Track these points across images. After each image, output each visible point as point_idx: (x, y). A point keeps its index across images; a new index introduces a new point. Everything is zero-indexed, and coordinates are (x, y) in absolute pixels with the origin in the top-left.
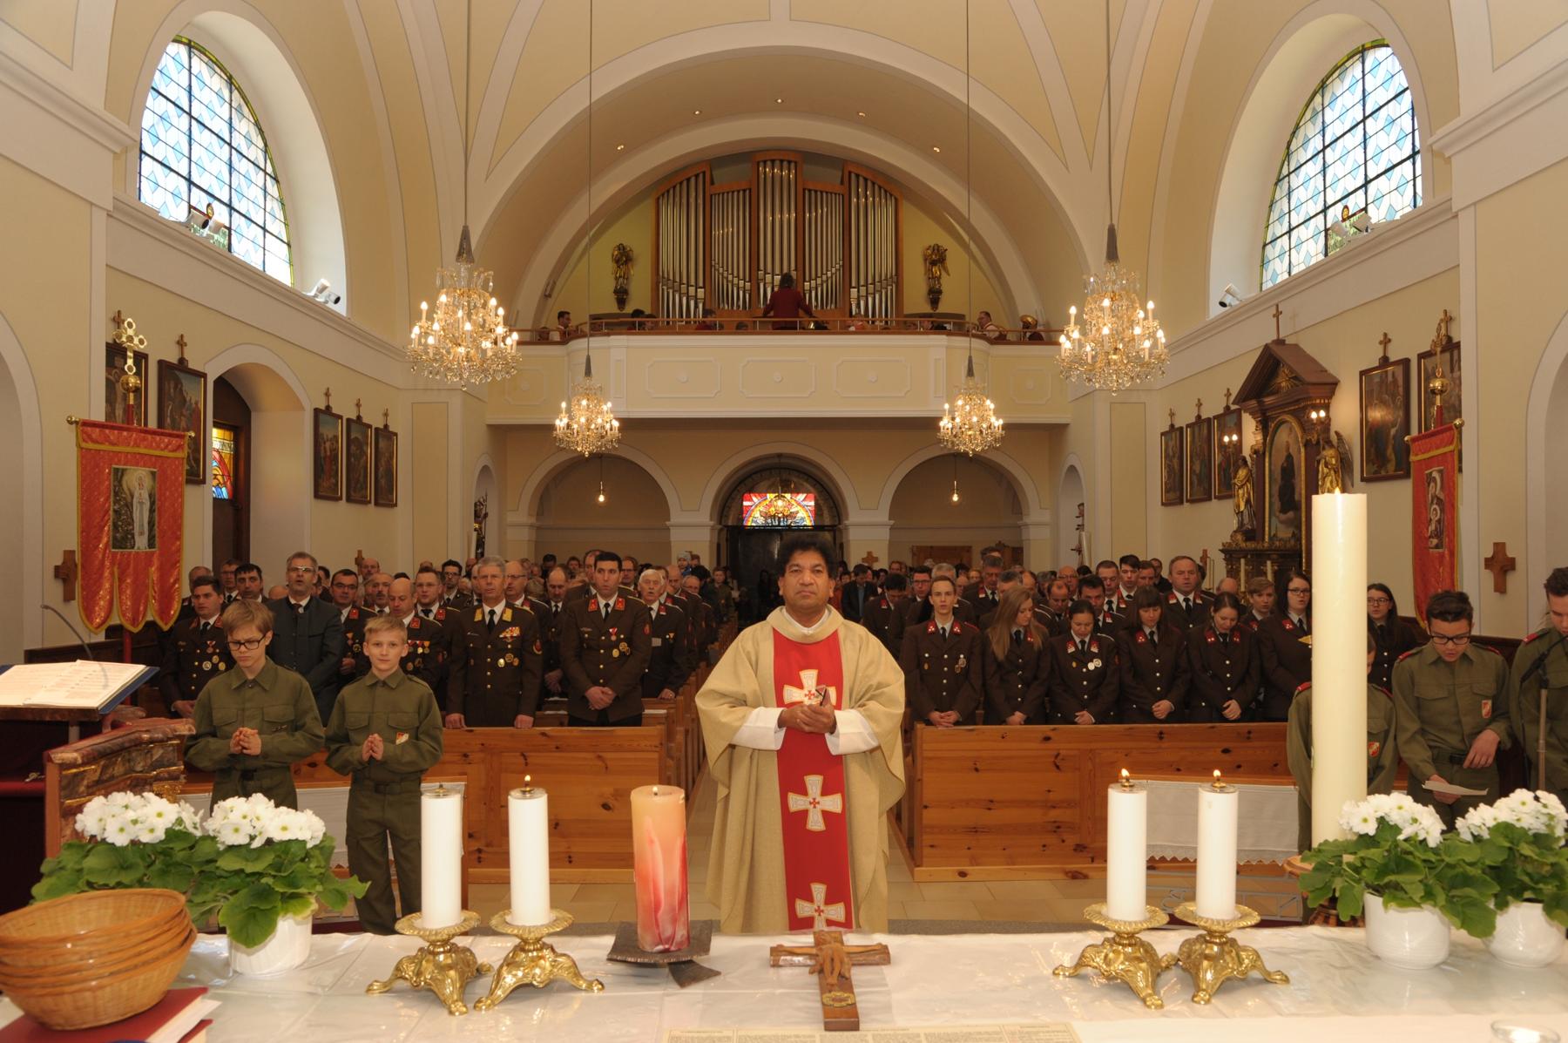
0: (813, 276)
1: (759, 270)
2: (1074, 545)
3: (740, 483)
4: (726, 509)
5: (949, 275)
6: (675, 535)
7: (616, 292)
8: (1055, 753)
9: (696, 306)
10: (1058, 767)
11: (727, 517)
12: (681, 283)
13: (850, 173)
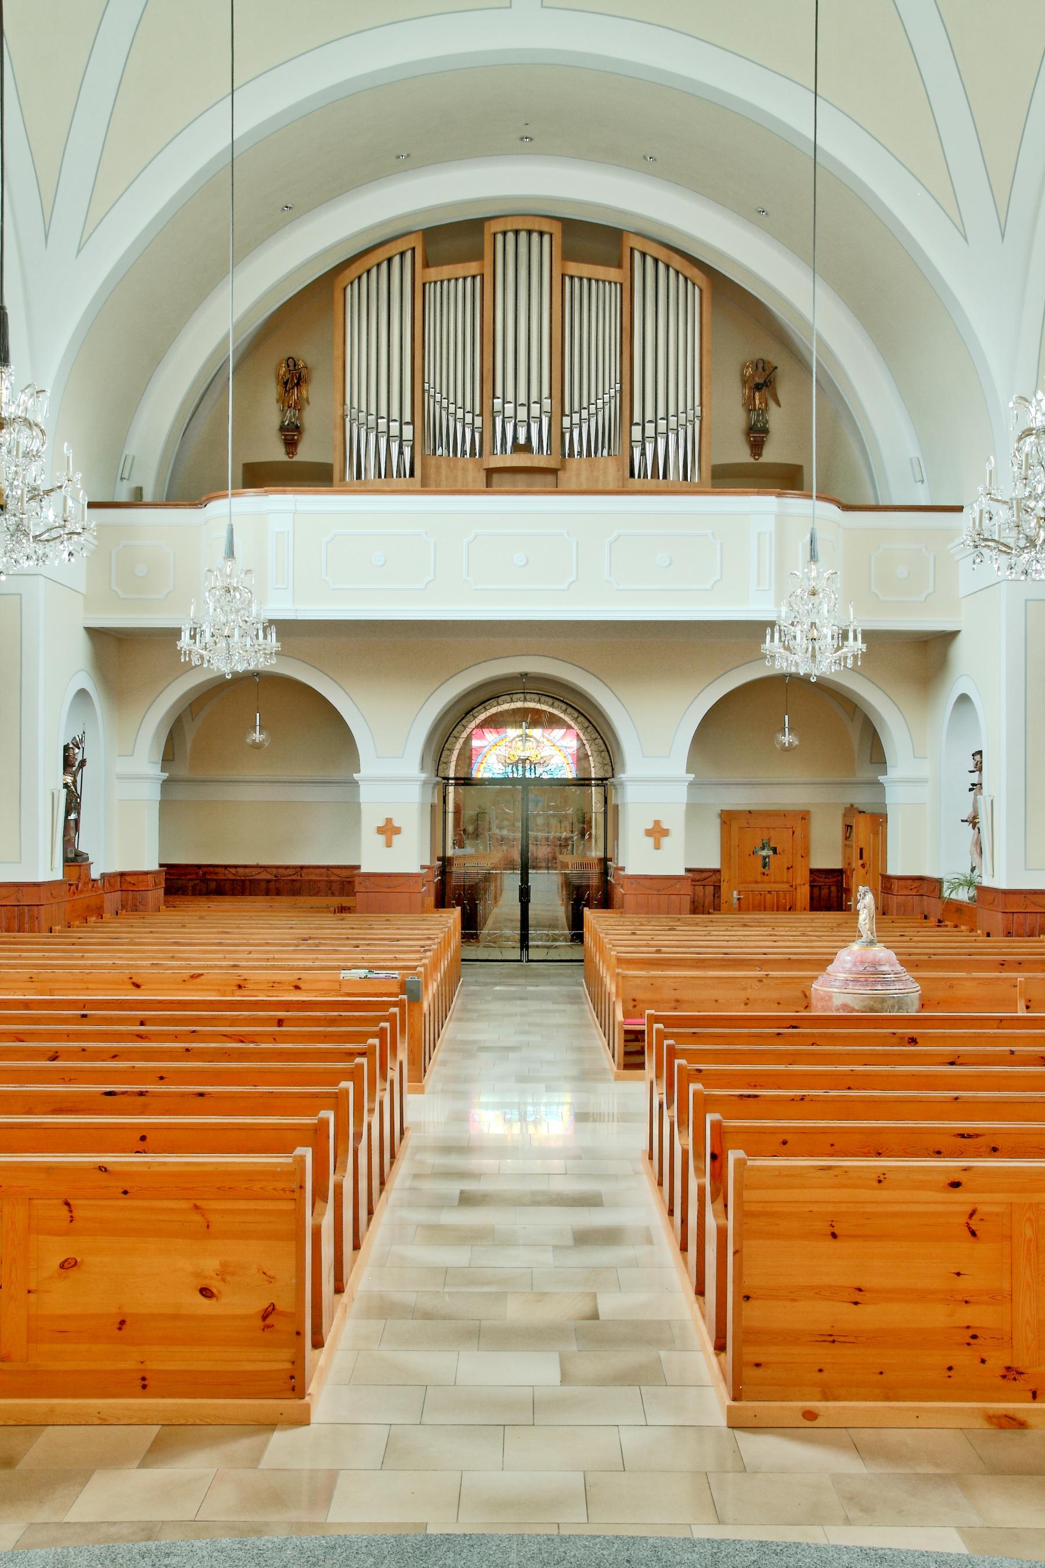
0: (576, 408)
1: (494, 397)
2: (967, 813)
3: (467, 714)
4: (445, 753)
5: (778, 404)
6: (367, 794)
7: (282, 429)
8: (968, 1209)
9: (401, 453)
10: (973, 1233)
11: (447, 763)
12: (359, 411)
13: (632, 250)
